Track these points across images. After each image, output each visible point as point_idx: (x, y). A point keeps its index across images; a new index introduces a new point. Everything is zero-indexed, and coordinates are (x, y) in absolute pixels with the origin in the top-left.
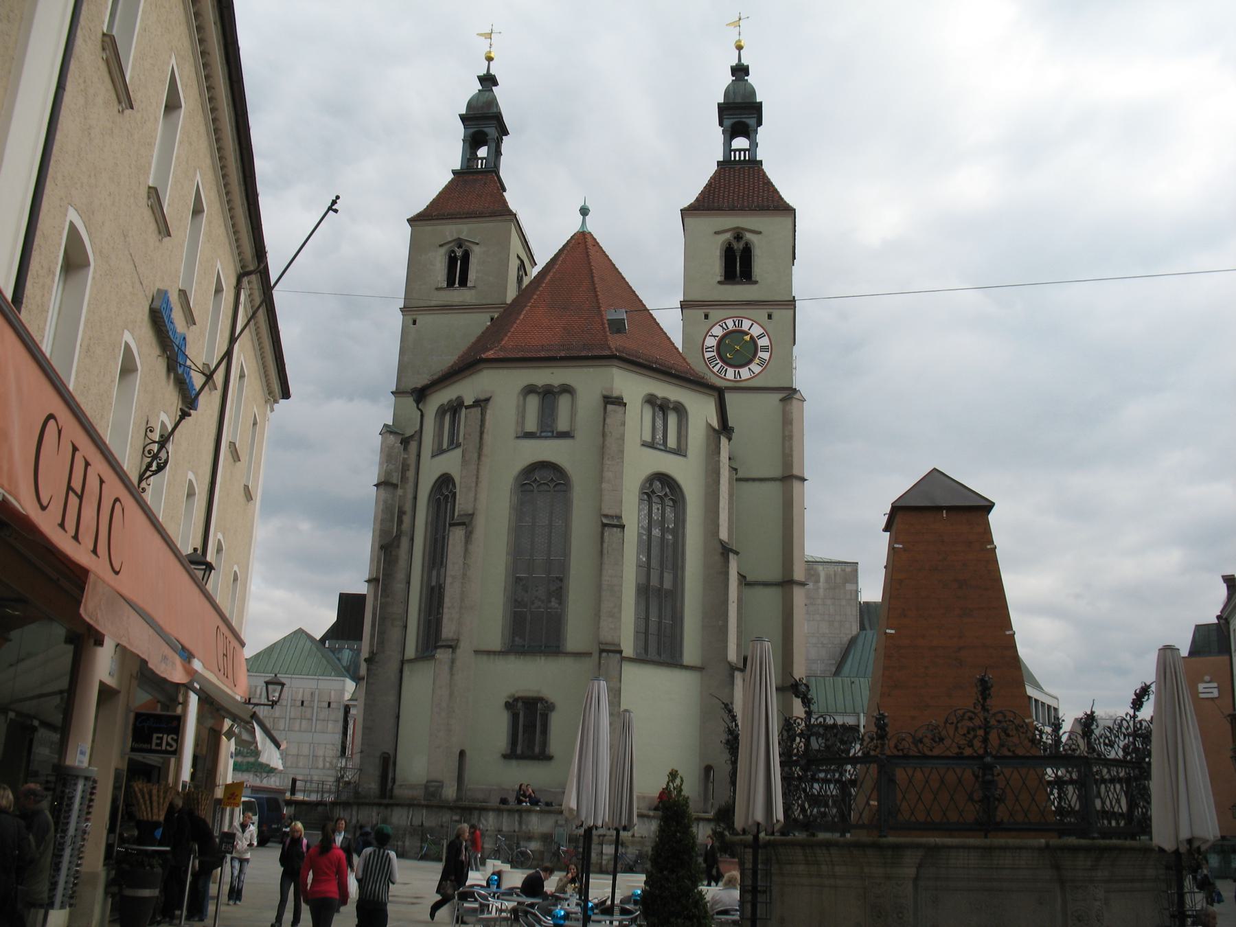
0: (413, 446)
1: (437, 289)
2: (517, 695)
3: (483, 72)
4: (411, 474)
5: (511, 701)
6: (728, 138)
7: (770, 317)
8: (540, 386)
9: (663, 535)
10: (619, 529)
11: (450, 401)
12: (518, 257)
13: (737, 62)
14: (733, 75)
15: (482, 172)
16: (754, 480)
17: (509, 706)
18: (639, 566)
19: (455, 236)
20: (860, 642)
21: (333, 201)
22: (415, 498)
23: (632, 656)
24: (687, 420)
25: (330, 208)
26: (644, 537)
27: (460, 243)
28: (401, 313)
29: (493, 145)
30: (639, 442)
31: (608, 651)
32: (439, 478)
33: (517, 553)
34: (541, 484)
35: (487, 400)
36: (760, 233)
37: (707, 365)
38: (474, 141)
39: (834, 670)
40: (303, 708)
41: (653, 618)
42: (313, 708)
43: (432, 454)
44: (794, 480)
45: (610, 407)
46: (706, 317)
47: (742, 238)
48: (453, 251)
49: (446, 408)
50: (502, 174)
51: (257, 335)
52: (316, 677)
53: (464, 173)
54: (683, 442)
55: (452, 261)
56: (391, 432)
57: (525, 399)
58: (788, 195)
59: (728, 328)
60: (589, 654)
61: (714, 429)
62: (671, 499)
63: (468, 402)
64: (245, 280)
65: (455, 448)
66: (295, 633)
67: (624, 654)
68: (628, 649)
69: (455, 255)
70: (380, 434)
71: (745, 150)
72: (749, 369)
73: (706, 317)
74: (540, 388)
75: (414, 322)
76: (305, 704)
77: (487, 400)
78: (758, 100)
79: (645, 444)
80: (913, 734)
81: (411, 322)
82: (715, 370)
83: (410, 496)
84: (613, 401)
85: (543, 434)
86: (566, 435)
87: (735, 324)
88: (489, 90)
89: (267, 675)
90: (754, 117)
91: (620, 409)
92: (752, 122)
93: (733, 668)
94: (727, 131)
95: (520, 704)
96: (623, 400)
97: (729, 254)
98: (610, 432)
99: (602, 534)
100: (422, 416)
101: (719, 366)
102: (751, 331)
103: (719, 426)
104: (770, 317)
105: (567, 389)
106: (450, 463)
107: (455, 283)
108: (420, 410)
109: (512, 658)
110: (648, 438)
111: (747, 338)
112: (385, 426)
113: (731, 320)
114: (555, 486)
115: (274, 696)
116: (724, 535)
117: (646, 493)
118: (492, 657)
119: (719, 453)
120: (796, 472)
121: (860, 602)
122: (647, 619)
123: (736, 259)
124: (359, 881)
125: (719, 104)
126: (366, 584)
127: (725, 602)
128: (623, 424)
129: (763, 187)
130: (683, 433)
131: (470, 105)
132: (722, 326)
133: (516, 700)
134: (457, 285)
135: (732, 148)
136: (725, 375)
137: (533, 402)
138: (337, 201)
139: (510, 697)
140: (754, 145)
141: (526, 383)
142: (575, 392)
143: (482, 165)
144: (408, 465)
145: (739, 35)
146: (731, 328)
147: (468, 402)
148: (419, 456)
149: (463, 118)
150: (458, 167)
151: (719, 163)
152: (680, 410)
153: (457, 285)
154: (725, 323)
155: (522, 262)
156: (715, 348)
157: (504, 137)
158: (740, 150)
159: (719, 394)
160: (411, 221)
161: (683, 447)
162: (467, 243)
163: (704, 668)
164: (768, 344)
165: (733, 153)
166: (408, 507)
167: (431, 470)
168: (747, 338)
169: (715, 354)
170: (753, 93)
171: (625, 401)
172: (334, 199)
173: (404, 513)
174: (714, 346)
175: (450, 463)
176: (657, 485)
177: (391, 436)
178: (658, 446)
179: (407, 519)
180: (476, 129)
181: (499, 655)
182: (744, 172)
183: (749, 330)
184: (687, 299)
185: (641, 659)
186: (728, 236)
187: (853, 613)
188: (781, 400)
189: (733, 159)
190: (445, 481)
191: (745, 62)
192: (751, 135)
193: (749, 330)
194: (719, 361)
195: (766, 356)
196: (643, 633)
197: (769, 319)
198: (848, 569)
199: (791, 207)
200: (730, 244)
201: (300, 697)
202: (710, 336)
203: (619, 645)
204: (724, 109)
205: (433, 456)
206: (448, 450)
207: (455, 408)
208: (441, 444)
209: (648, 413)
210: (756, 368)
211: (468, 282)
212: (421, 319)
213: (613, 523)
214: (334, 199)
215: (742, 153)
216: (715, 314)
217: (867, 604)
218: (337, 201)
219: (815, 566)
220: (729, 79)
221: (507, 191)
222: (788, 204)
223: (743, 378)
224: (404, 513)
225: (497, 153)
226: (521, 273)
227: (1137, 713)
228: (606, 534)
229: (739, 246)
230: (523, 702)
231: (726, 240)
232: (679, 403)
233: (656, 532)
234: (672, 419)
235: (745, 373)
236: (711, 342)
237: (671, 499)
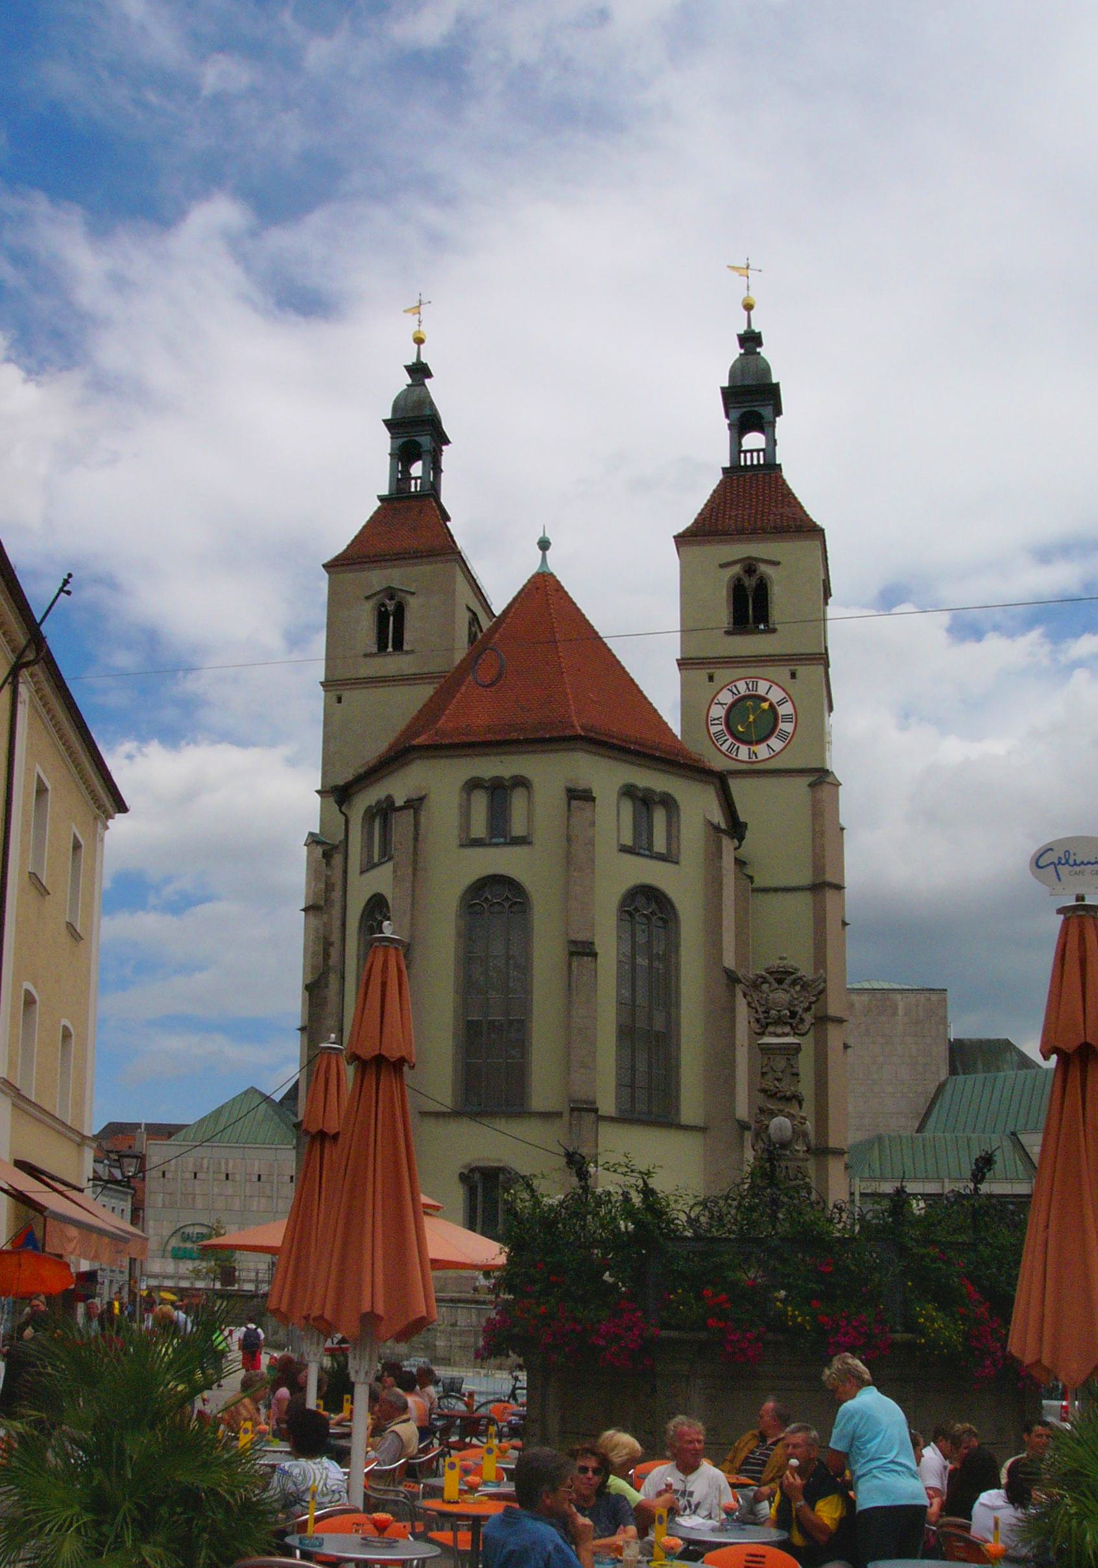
0: (338, 859)
1: (366, 656)
2: (474, 1165)
3: (411, 360)
4: (336, 895)
5: (466, 1172)
6: (736, 435)
7: (793, 675)
8: (487, 779)
9: (651, 962)
10: (590, 959)
11: (379, 802)
12: (469, 609)
13: (745, 328)
14: (742, 346)
15: (417, 497)
16: (776, 890)
17: (463, 1178)
18: (620, 1003)
19: (384, 586)
20: (949, 1087)
21: (64, 580)
22: (344, 925)
23: (613, 1115)
24: (679, 815)
25: (61, 590)
26: (627, 967)
27: (390, 593)
28: (322, 688)
29: (429, 459)
30: (615, 847)
31: (580, 1110)
32: (370, 900)
33: (468, 987)
34: (516, 903)
35: (421, 799)
36: (778, 563)
37: (713, 743)
38: (404, 454)
39: (917, 1125)
40: (197, 1182)
41: (642, 1067)
42: (272, 1183)
43: (361, 868)
44: (827, 889)
45: (574, 803)
46: (711, 678)
47: (755, 571)
48: (383, 605)
49: (375, 811)
50: (444, 500)
51: (61, 738)
52: (273, 1146)
53: (397, 499)
54: (674, 846)
55: (382, 618)
56: (318, 843)
57: (469, 794)
58: (816, 512)
59: (739, 693)
60: (559, 1115)
61: (717, 828)
62: (662, 919)
63: (399, 803)
64: (25, 674)
65: (387, 861)
66: (246, 1093)
67: (600, 1113)
68: (607, 1105)
69: (386, 610)
70: (305, 845)
71: (758, 451)
72: (768, 745)
73: (711, 678)
74: (508, 780)
75: (339, 700)
76: (262, 1178)
77: (421, 799)
78: (774, 381)
79: (624, 849)
80: (688, 1212)
81: (335, 699)
82: (724, 748)
83: (337, 923)
84: (579, 796)
85: (495, 840)
86: (523, 841)
87: (748, 688)
88: (419, 385)
89: (187, 1143)
90: (770, 405)
91: (588, 805)
92: (766, 412)
93: (744, 1126)
94: (733, 425)
95: (477, 1176)
96: (592, 793)
97: (738, 592)
98: (577, 836)
99: (570, 965)
100: (347, 822)
101: (729, 743)
102: (769, 696)
103: (727, 822)
104: (793, 675)
105: (521, 782)
106: (381, 880)
107: (387, 647)
108: (345, 814)
109: (465, 1120)
110: (628, 840)
111: (765, 705)
112: (311, 834)
113: (743, 682)
114: (510, 907)
115: (129, 1172)
116: (729, 961)
117: (626, 911)
118: (441, 1121)
119: (721, 858)
120: (829, 877)
121: (949, 1040)
122: (633, 1069)
123: (748, 601)
124: (399, 1387)
125: (723, 389)
126: (299, 1032)
127: (732, 1046)
128: (593, 824)
129: (783, 500)
130: (674, 832)
131: (396, 407)
132: (731, 691)
133: (472, 1170)
134: (390, 649)
135: (743, 449)
136: (736, 755)
137: (480, 802)
138: (70, 580)
139: (464, 1167)
140: (772, 442)
141: (467, 777)
142: (531, 785)
143: (416, 487)
144: (333, 885)
145: (748, 290)
146: (743, 693)
147: (399, 803)
148: (345, 872)
149: (388, 424)
150: (385, 492)
151: (725, 470)
152: (668, 802)
153: (390, 649)
154: (735, 686)
155: (474, 614)
156: (723, 720)
157: (444, 448)
158: (751, 451)
159: (721, 781)
160: (328, 566)
161: (674, 851)
162: (400, 593)
163: (706, 1129)
164: (791, 711)
165: (742, 455)
166: (335, 937)
167: (362, 888)
168: (765, 705)
169: (723, 727)
170: (767, 371)
171: (594, 795)
172: (66, 577)
173: (331, 944)
174: (721, 718)
175: (381, 880)
176: (641, 901)
177: (319, 847)
178: (642, 851)
179: (334, 953)
180: (406, 439)
181: (449, 1117)
182: (757, 481)
183: (767, 693)
184: (685, 656)
185: (626, 1118)
186: (737, 569)
187: (942, 1052)
188: (810, 785)
189: (742, 464)
190: (377, 907)
191: (756, 328)
192: (766, 429)
193: (767, 693)
194: (728, 737)
195: (787, 727)
196: (628, 1084)
197: (792, 678)
198: (934, 997)
199: (818, 526)
200: (739, 580)
201: (256, 1171)
202: (716, 704)
203: (595, 1102)
204: (731, 396)
205: (362, 872)
206: (380, 864)
207: (384, 811)
208: (371, 857)
209: (627, 808)
210: (775, 743)
211: (405, 644)
212: (346, 695)
213: (583, 950)
214: (66, 577)
215: (755, 454)
216: (723, 675)
217: (959, 1042)
218: (70, 580)
219: (890, 995)
220: (736, 351)
221: (452, 520)
222: (814, 523)
223: (760, 758)
224: (331, 944)
225: (436, 467)
226: (473, 629)
227: (979, 1186)
228: (574, 964)
229: (750, 583)
230: (482, 1174)
231: (732, 577)
232: (669, 795)
233: (642, 961)
234: (659, 817)
235: (762, 751)
236: (718, 712)
237: (662, 919)
